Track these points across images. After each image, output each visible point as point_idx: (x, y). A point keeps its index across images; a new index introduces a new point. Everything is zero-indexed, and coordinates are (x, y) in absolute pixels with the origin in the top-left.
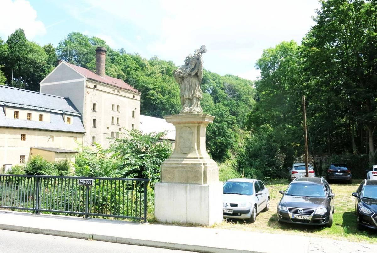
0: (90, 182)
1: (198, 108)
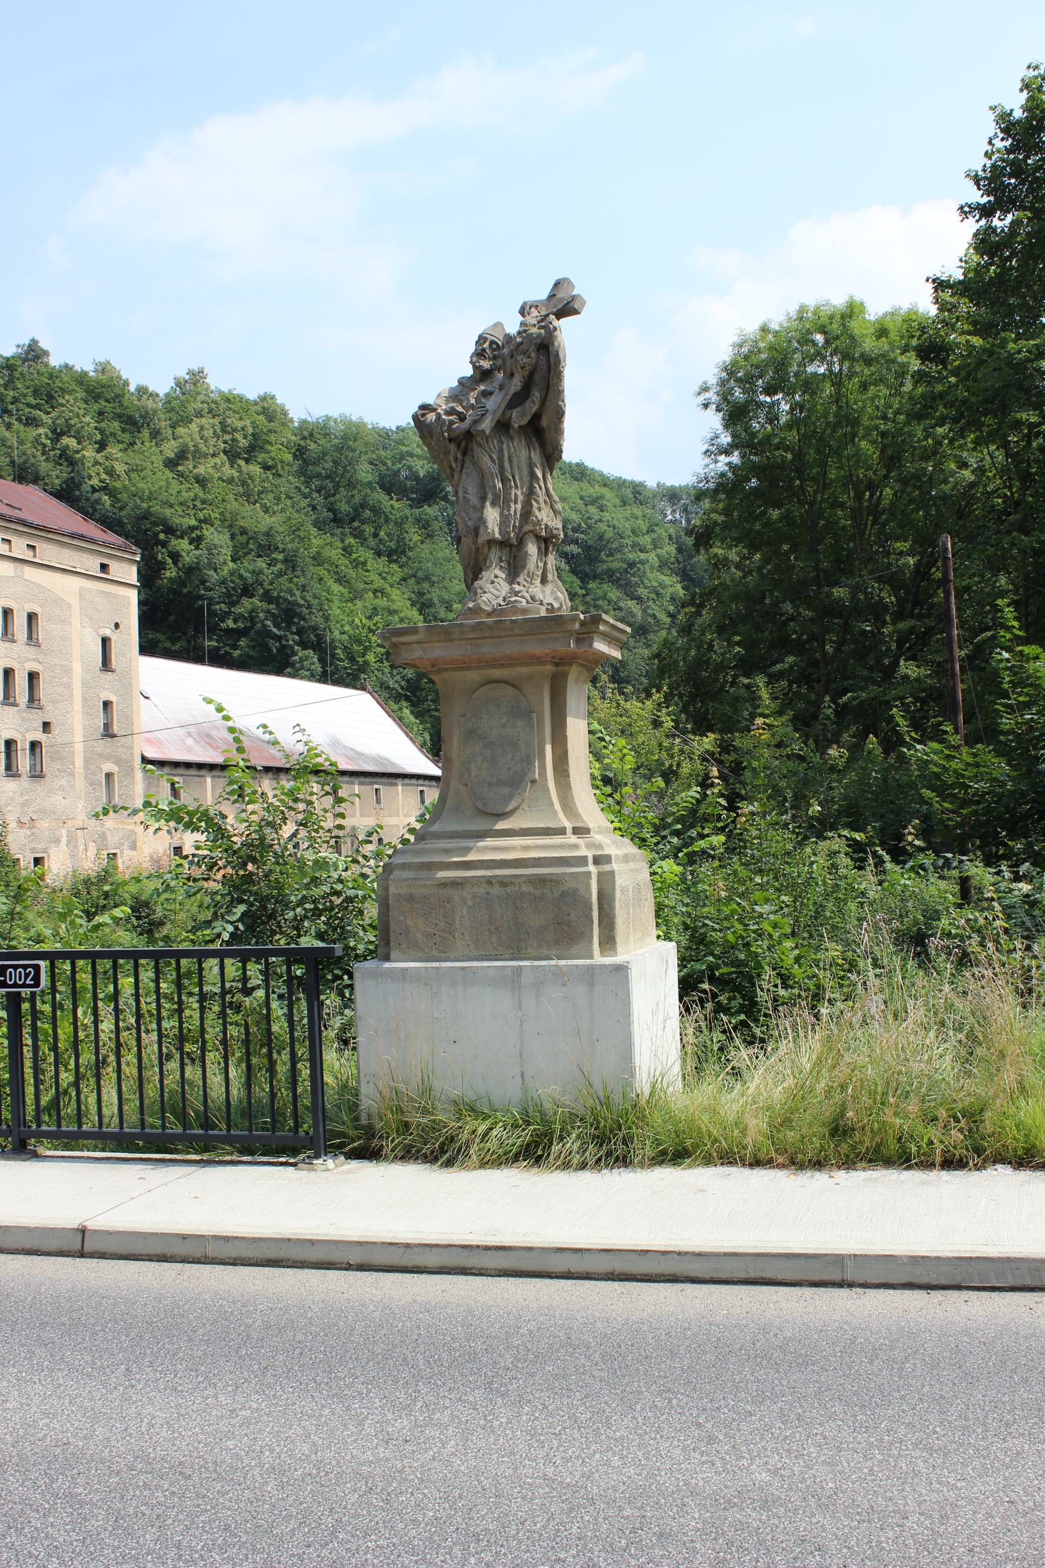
0: (27, 976)
1: (549, 588)
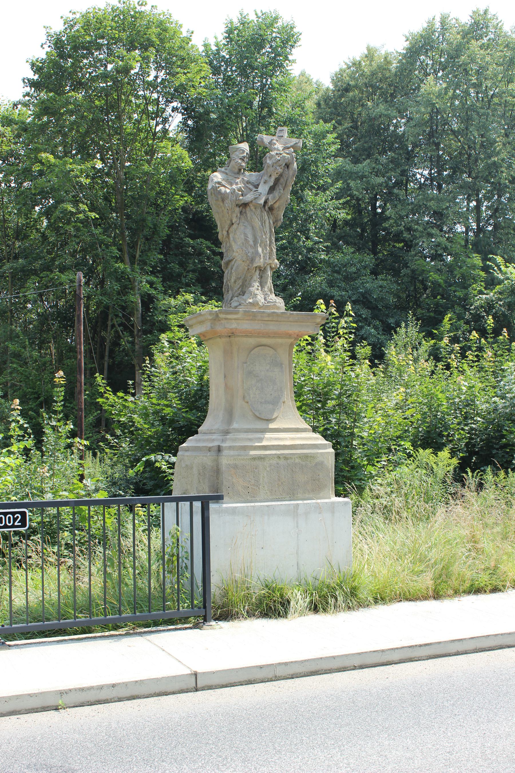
0: (15, 520)
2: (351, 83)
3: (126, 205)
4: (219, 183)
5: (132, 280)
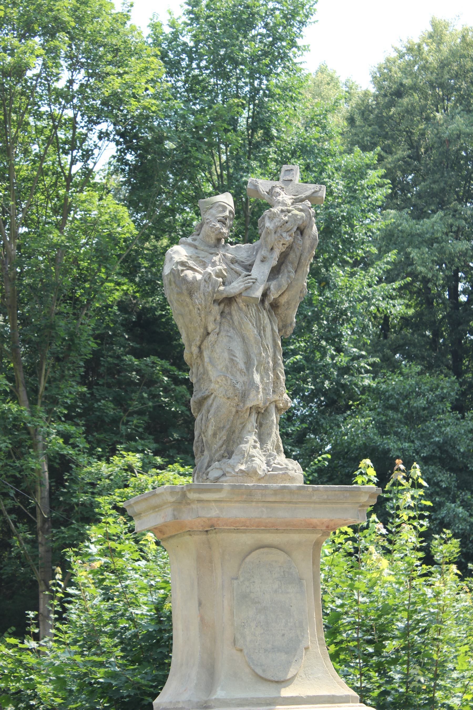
2: (405, 81)
3: (20, 301)
4: (183, 264)
5: (32, 432)
